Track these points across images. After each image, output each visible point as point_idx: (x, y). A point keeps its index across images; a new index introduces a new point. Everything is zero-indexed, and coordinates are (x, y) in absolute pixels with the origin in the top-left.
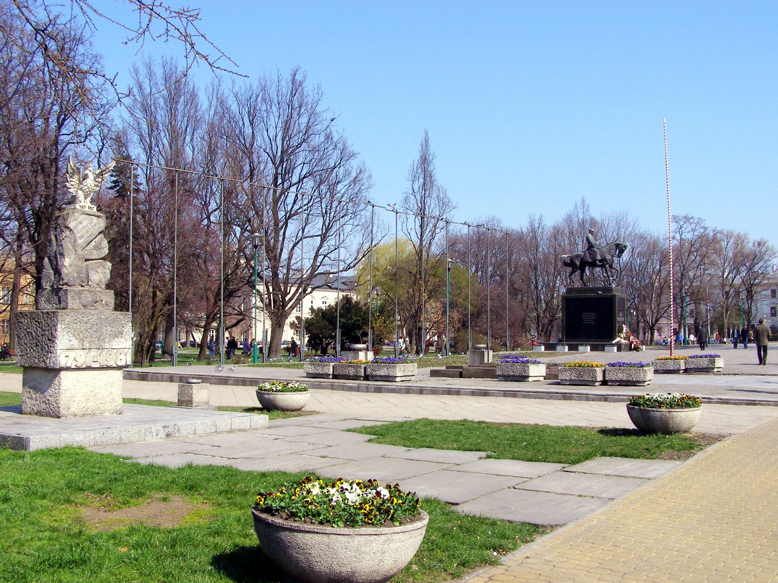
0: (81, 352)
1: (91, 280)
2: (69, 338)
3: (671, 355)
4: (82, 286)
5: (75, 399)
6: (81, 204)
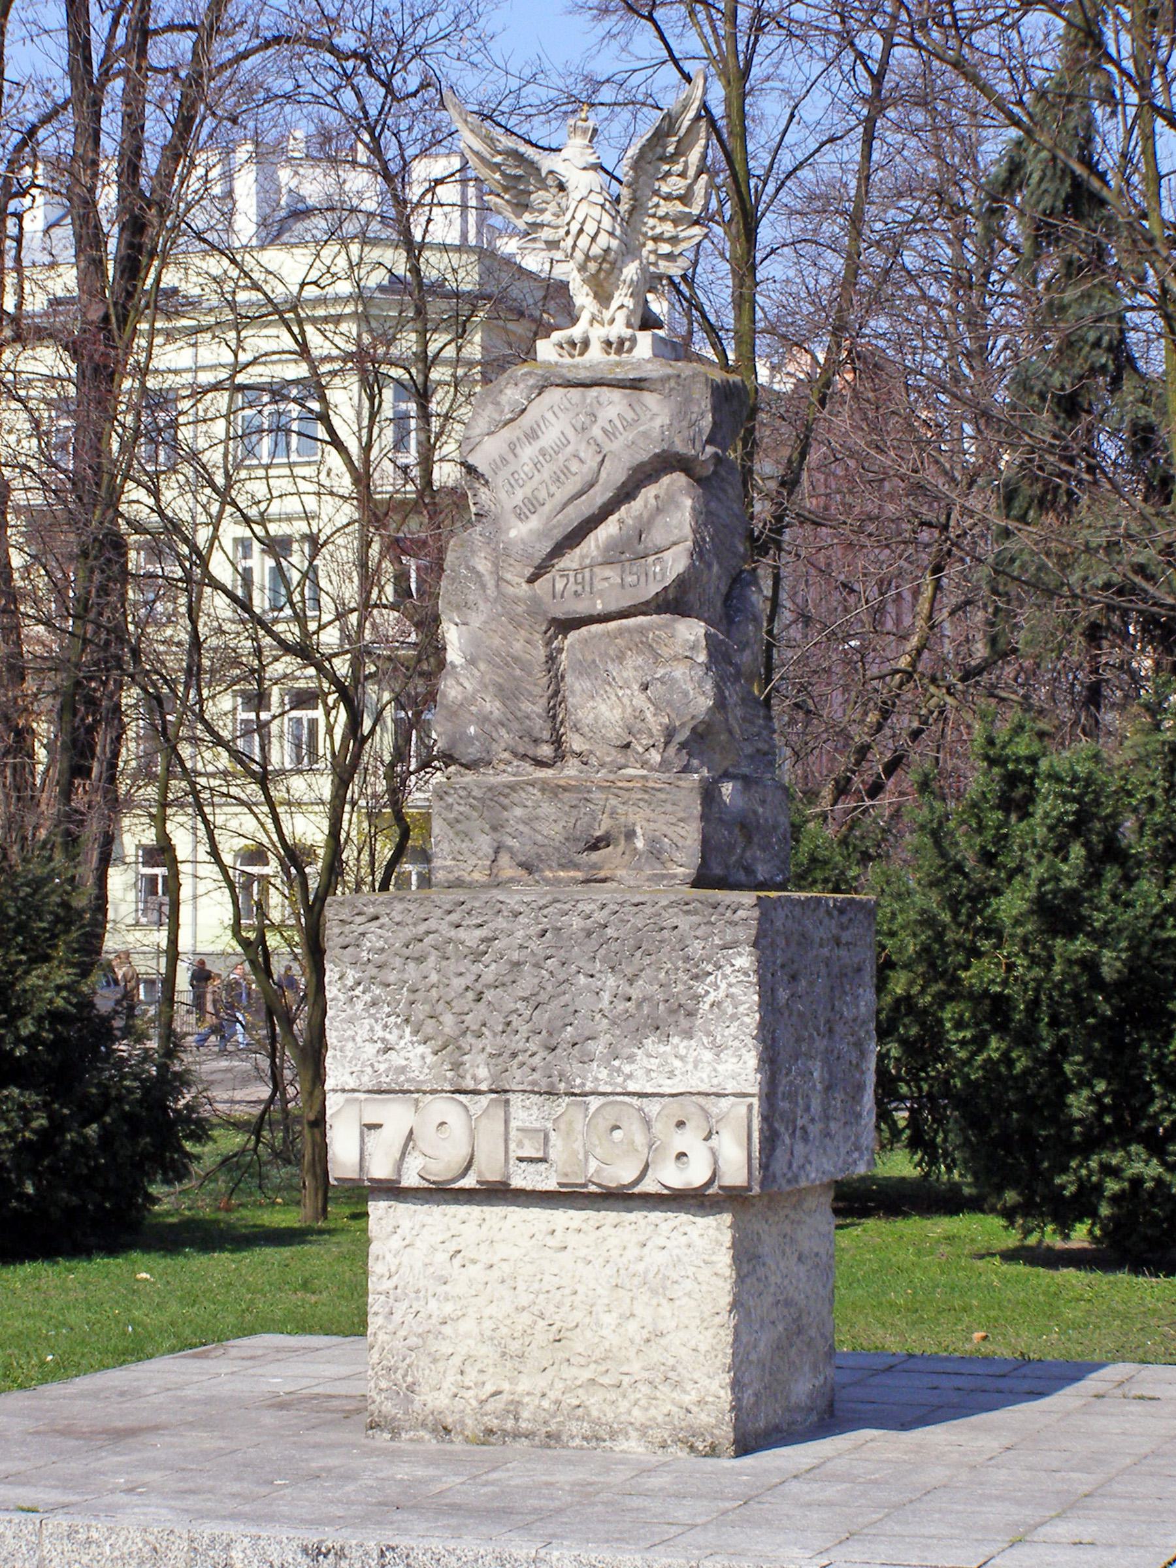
0: (443, 1108)
1: (576, 729)
2: (379, 1033)
3: (521, 1160)
5: (445, 1348)
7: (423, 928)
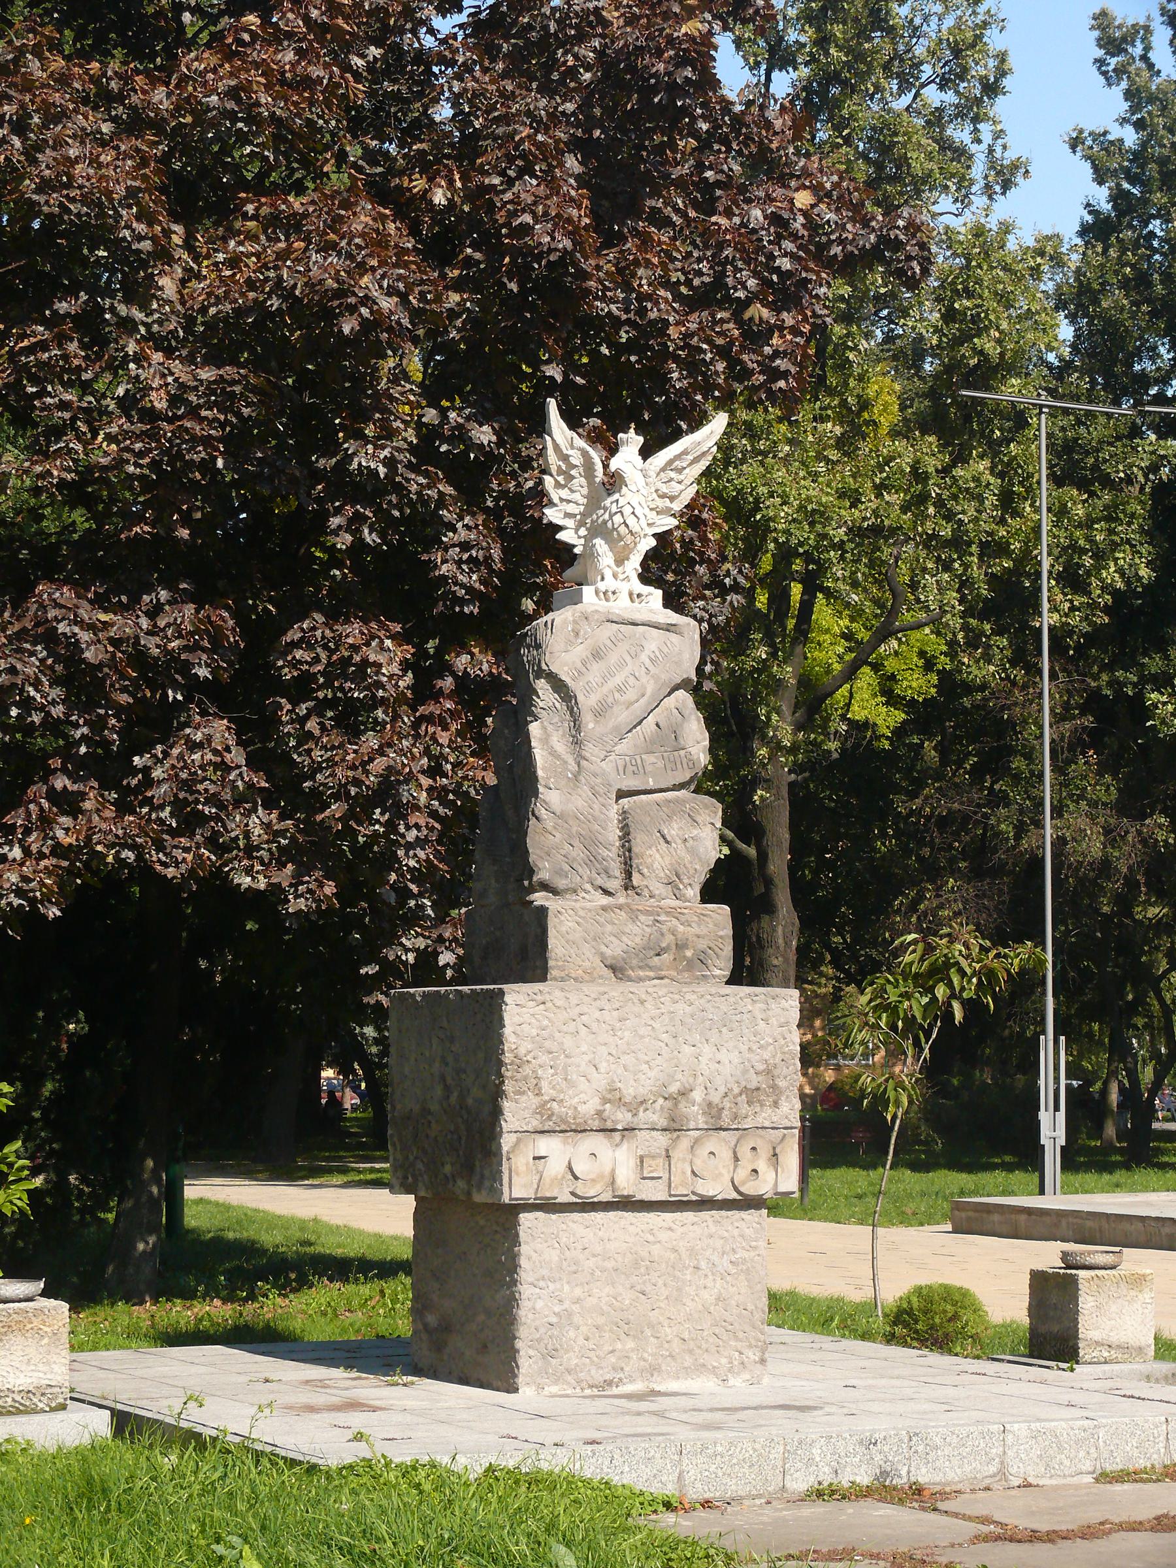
4: (606, 892)
6: (602, 586)
7: (577, 1010)
